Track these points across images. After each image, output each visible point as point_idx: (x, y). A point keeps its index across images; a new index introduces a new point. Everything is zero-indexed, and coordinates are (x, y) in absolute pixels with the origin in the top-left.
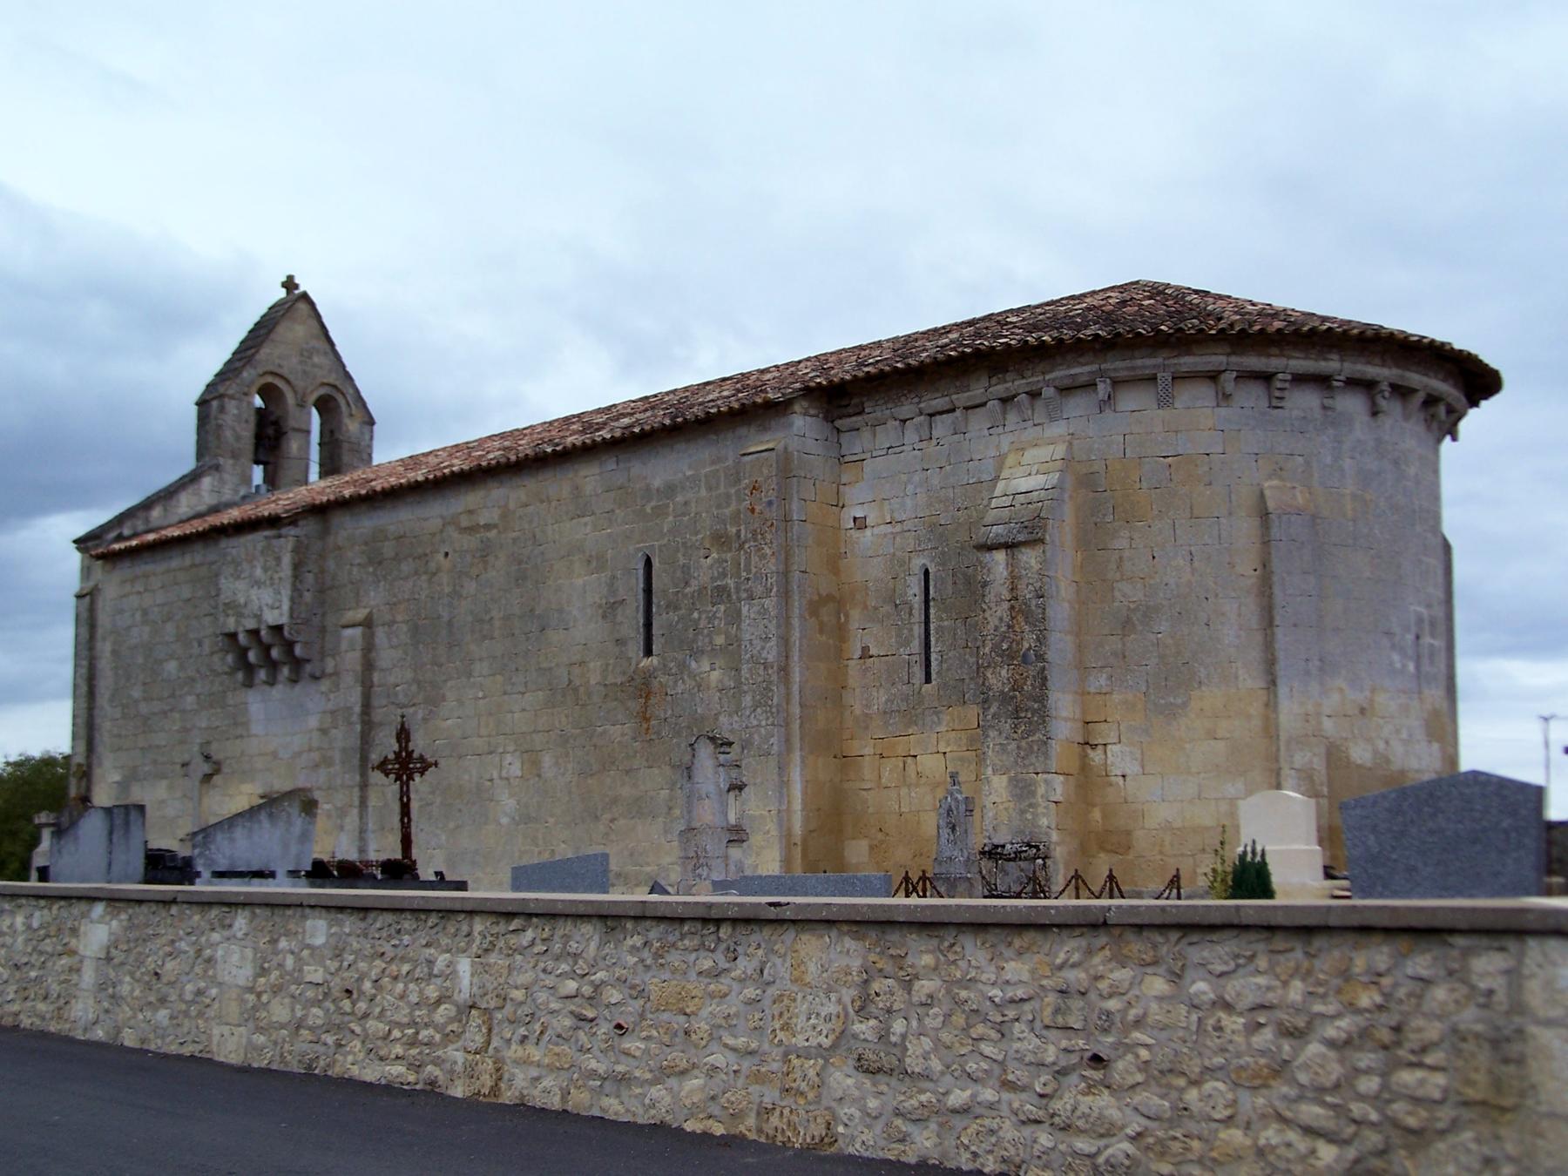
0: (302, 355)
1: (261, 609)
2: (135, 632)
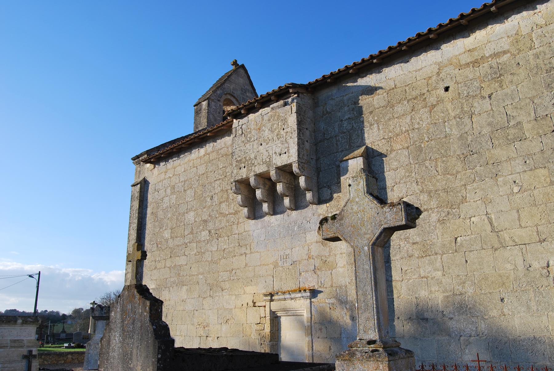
0: (242, 91)
1: (270, 157)
2: (166, 200)
